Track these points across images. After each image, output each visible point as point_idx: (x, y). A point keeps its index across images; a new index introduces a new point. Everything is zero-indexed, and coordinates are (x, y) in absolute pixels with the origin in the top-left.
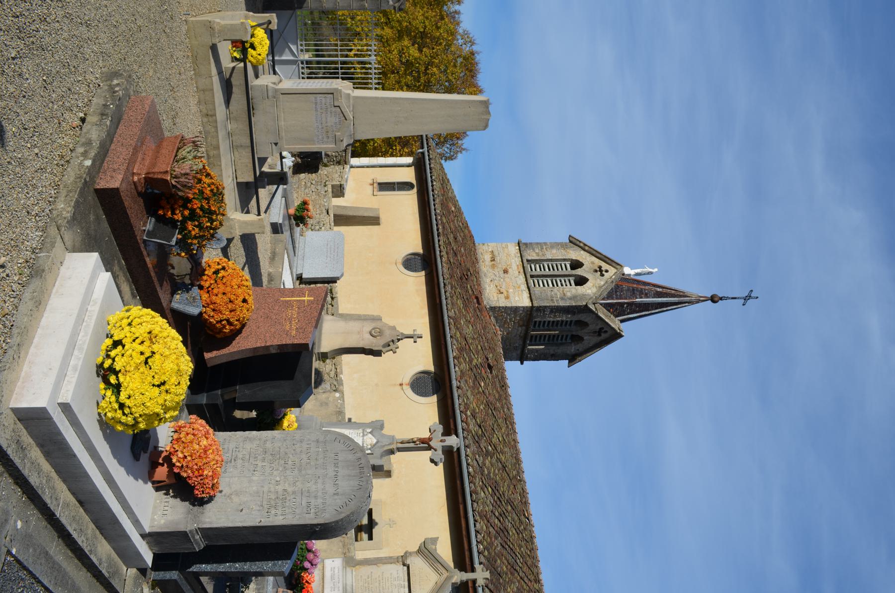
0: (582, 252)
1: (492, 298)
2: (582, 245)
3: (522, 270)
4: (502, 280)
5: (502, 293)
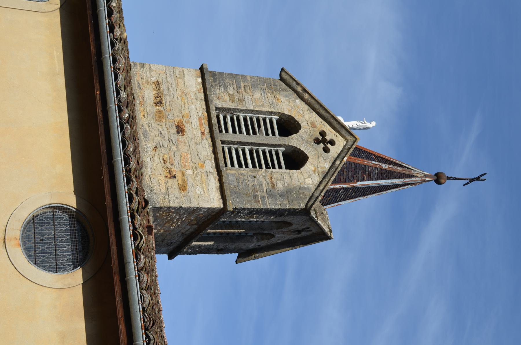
0: (298, 101)
1: (156, 187)
2: (299, 89)
3: (207, 130)
4: (174, 148)
5: (174, 177)
